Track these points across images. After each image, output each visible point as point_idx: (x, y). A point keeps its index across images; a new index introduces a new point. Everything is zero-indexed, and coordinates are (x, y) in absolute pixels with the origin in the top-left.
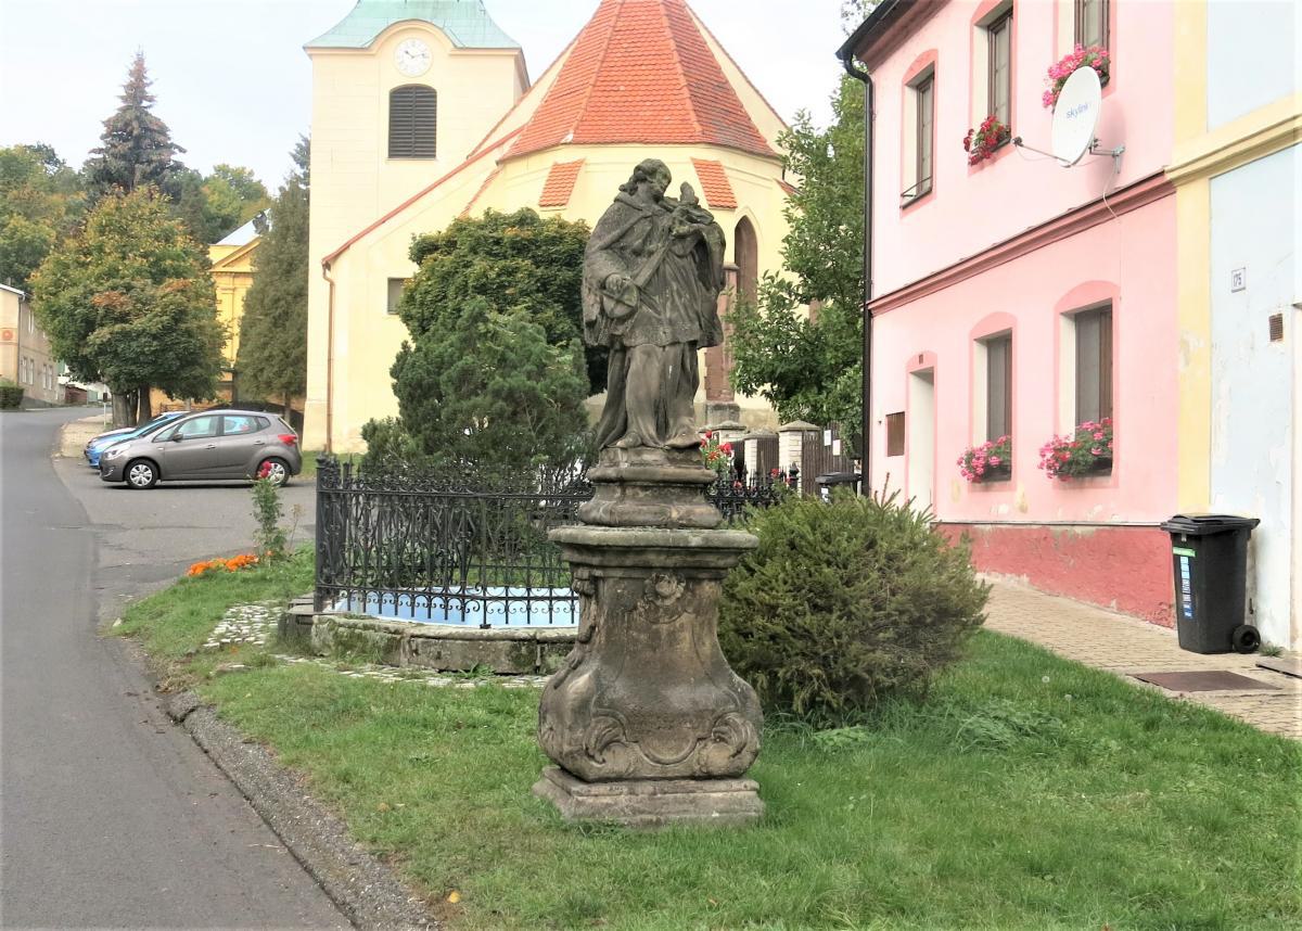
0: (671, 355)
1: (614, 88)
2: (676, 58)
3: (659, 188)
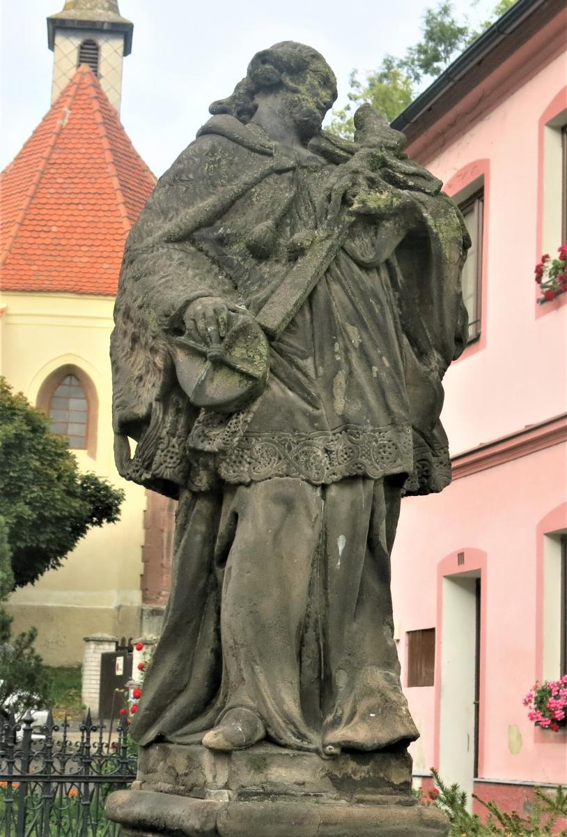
0: (344, 509)
1: (45, 229)
2: (120, 198)
3: (312, 106)
